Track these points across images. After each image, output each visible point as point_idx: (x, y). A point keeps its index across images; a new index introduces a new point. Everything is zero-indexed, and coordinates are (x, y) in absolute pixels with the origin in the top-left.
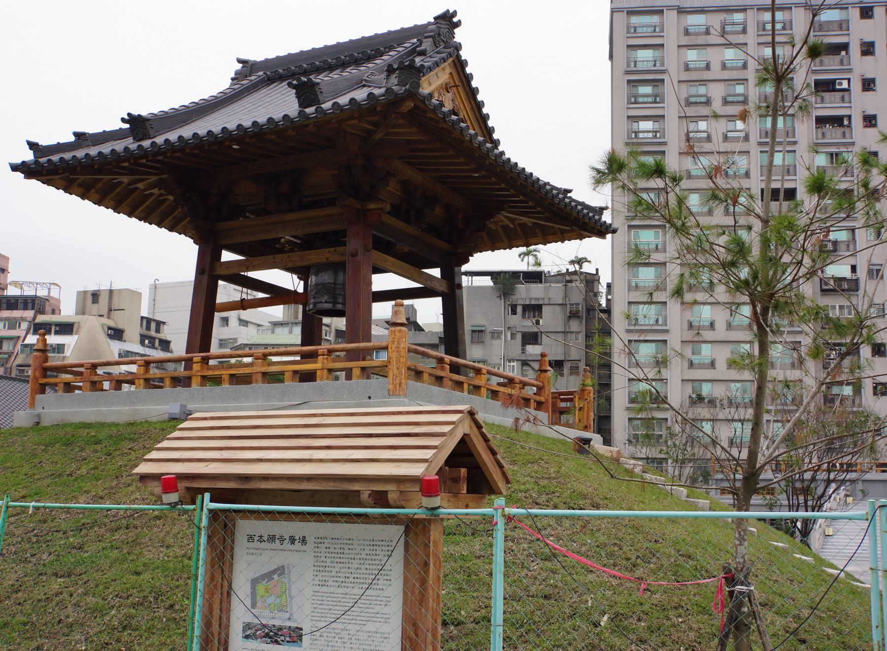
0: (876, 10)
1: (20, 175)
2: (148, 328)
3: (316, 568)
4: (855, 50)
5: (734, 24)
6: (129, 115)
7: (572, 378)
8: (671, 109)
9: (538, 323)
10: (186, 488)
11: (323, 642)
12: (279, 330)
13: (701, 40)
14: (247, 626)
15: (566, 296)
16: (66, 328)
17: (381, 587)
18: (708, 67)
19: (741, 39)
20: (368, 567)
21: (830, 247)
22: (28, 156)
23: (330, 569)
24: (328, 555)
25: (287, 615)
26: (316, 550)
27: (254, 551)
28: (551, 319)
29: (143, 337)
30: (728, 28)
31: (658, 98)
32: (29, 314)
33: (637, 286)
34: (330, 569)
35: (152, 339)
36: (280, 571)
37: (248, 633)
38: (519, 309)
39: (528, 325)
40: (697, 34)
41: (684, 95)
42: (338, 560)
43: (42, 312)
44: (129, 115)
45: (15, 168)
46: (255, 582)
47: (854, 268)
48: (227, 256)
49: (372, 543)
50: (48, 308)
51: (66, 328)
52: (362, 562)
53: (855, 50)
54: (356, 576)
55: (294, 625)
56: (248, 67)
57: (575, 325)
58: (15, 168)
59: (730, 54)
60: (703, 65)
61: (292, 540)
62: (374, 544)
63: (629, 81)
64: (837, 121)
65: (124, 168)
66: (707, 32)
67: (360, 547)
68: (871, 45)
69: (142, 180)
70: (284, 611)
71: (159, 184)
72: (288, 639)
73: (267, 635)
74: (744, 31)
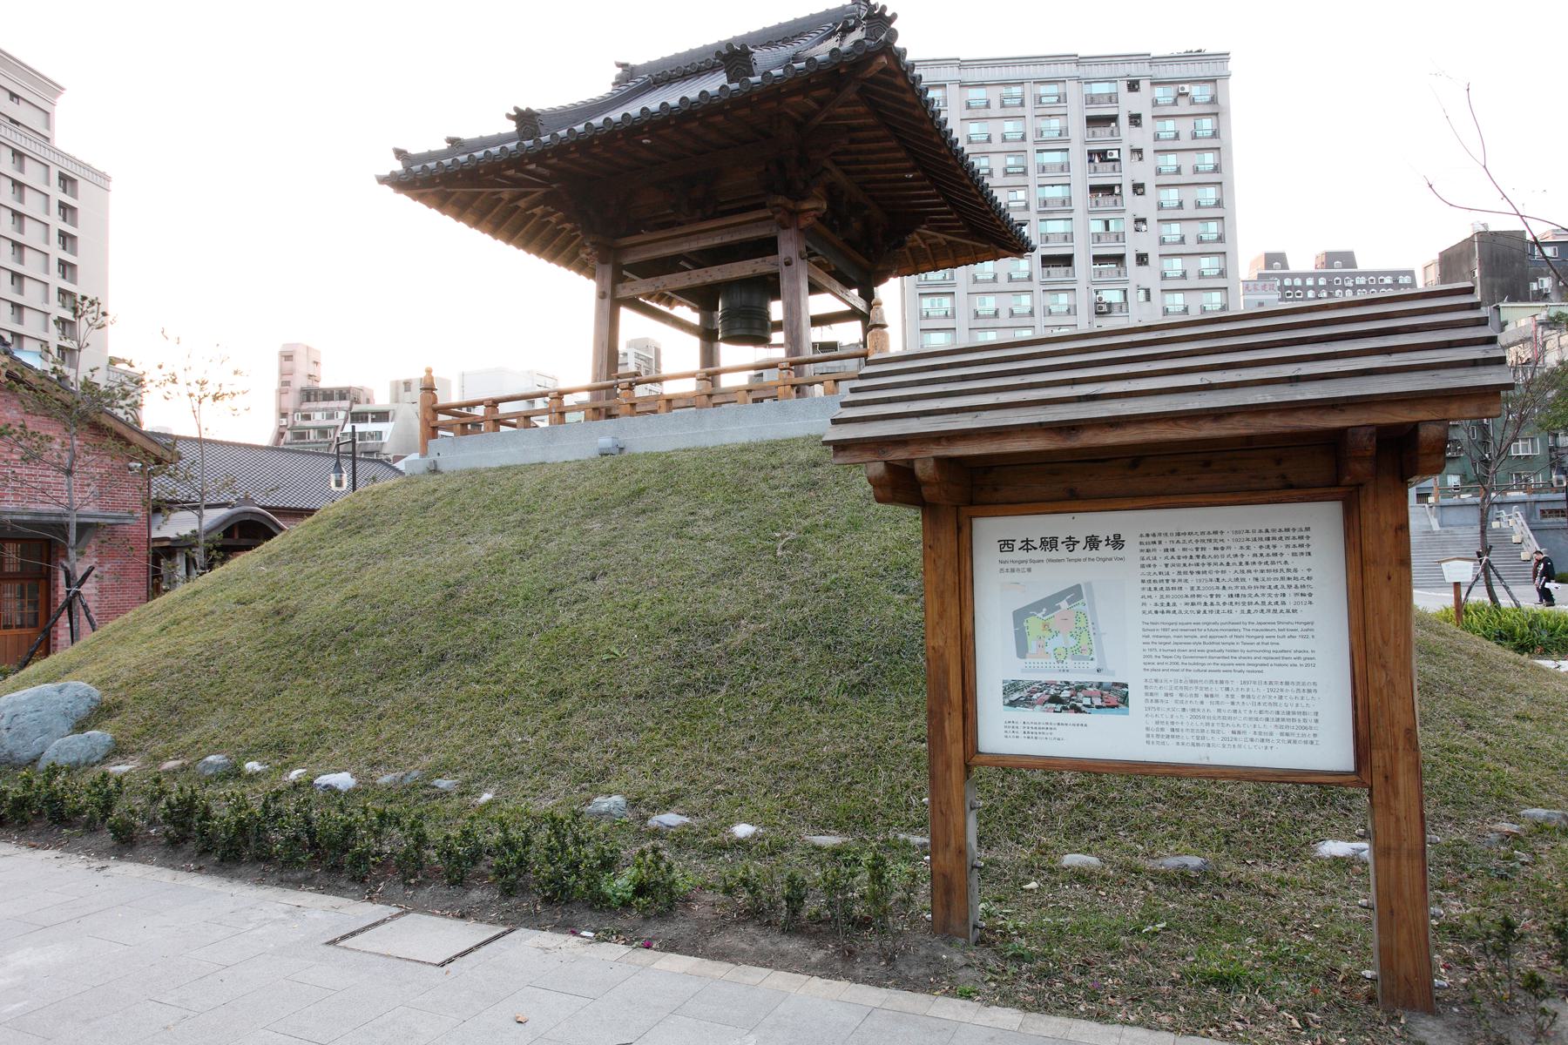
1: (388, 190)
3: (1146, 585)
4: (1124, 120)
6: (516, 109)
10: (938, 460)
11: (1171, 704)
13: (982, 113)
14: (1011, 687)
16: (382, 416)
17: (1292, 607)
18: (989, 140)
19: (1019, 112)
20: (1259, 575)
21: (1105, 309)
22: (398, 166)
23: (1177, 585)
24: (1170, 562)
25: (1094, 665)
26: (1146, 555)
27: (1016, 566)
32: (346, 404)
34: (1177, 585)
36: (1075, 593)
37: (1016, 696)
40: (978, 108)
42: (1195, 569)
43: (358, 402)
44: (516, 109)
45: (383, 180)
46: (1020, 616)
49: (1264, 535)
50: (363, 399)
51: (382, 416)
52: (1245, 568)
53: (1124, 120)
54: (1234, 592)
55: (1107, 679)
56: (628, 72)
58: (383, 180)
59: (1009, 126)
61: (1071, 543)
62: (1268, 536)
64: (1108, 190)
65: (507, 178)
66: (988, 106)
67: (1238, 544)
68: (1138, 116)
69: (525, 195)
70: (1085, 658)
71: (545, 200)
72: (1098, 702)
73: (1055, 699)
74: (1022, 104)
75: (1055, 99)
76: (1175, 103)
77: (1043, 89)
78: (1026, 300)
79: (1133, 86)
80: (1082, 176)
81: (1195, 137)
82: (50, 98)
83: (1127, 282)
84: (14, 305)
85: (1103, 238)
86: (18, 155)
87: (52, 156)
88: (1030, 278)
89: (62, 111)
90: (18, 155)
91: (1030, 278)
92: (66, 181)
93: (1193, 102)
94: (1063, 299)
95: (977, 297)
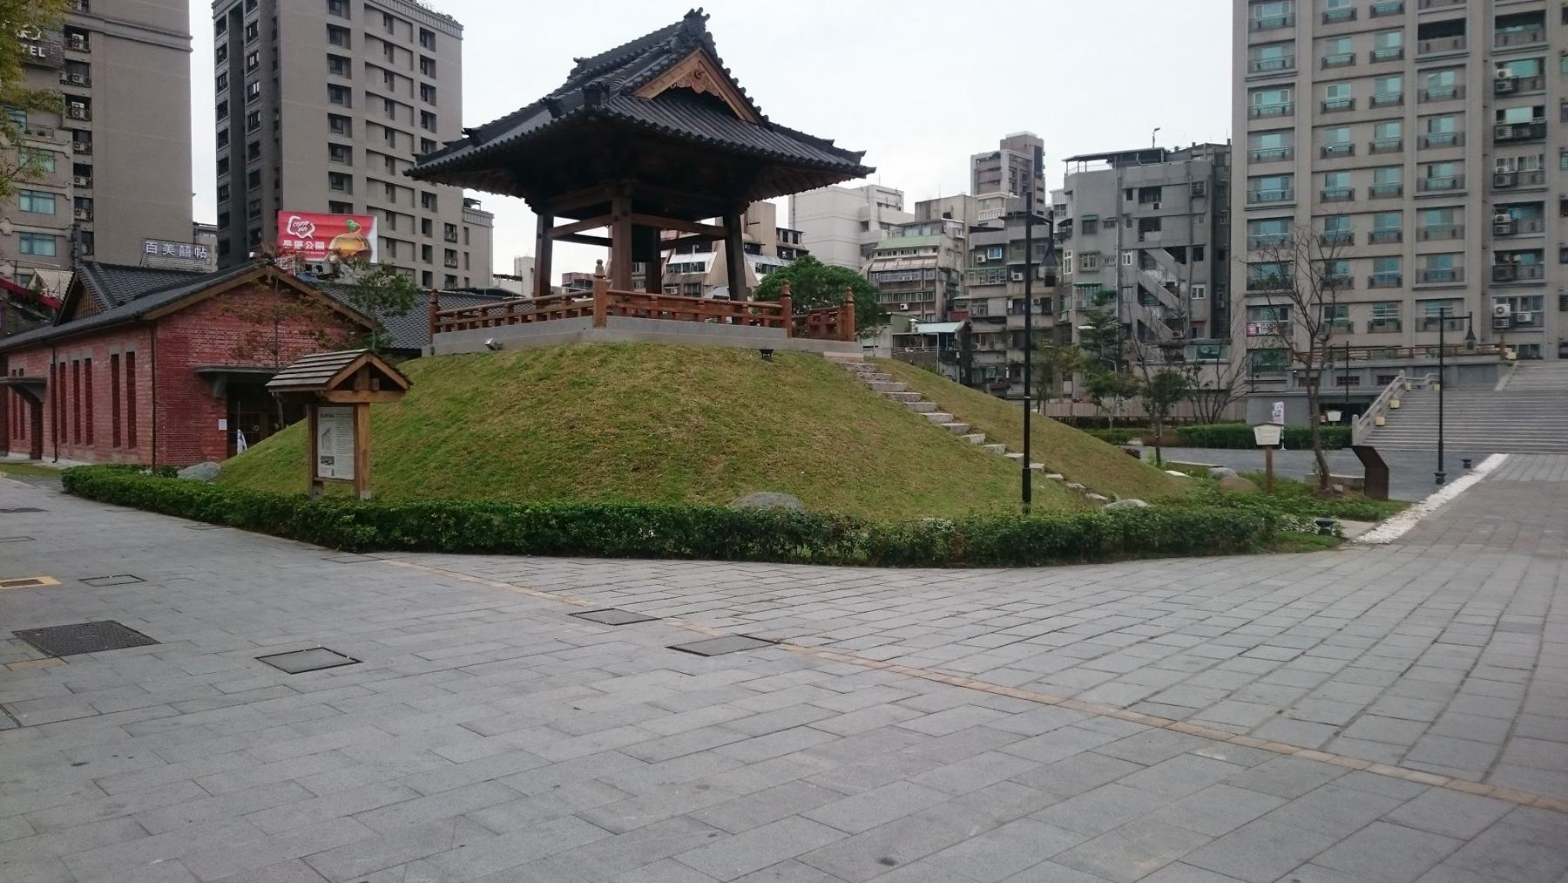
2: (786, 239)
7: (1197, 264)
9: (1156, 207)
12: (909, 232)
15: (1188, 174)
28: (1172, 200)
29: (780, 249)
33: (1259, 158)
35: (789, 250)
38: (1136, 194)
39: (1148, 210)
47: (1538, 111)
48: (559, 222)
57: (1199, 206)
78: (1394, 85)
83: (1545, 48)
84: (388, 212)
88: (1401, 56)
91: (1401, 56)
92: (427, 36)
94: (1448, 79)
95: (1326, 88)
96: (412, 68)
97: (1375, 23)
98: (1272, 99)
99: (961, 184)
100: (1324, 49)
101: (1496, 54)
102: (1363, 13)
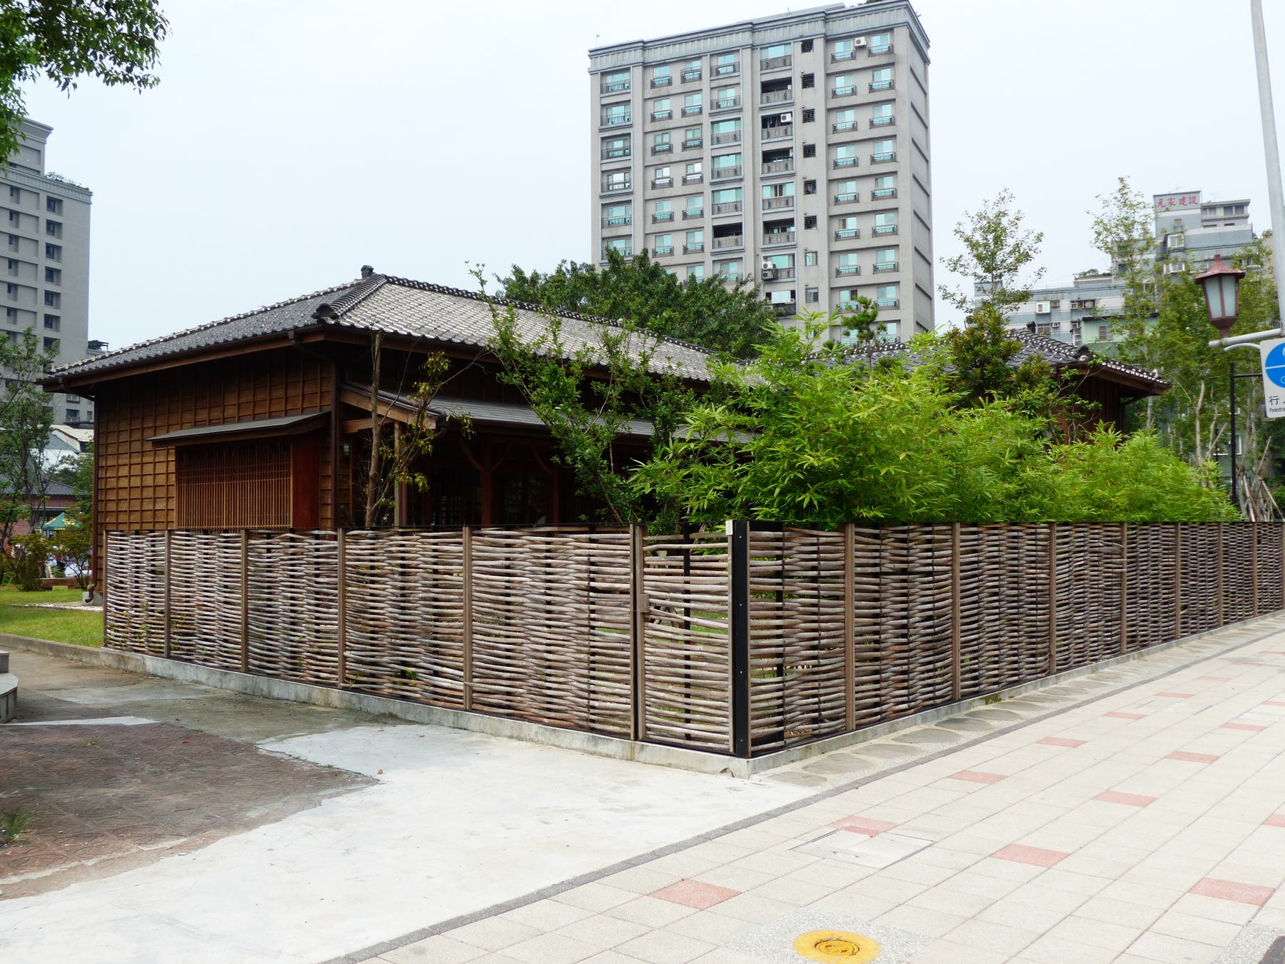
0: (815, 42)
5: (693, 71)
8: (636, 162)
13: (664, 91)
22: (528, 275)
30: (688, 76)
31: (626, 152)
41: (650, 144)
47: (793, 294)
60: (849, 91)
63: (603, 139)
64: (784, 153)
66: (670, 83)
74: (700, 78)
75: (731, 69)
76: (853, 57)
77: (721, 60)
79: (807, 46)
80: (753, 141)
81: (871, 89)
82: (41, 139)
83: (795, 246)
85: (774, 205)
86: (15, 191)
87: (42, 186)
89: (52, 147)
90: (15, 191)
91: (701, 180)
92: (53, 204)
93: (870, 54)
96: (37, 231)
97: (685, 224)
98: (618, 212)
99: (324, 802)
100: (651, 207)
101: (764, 250)
102: (678, 217)
